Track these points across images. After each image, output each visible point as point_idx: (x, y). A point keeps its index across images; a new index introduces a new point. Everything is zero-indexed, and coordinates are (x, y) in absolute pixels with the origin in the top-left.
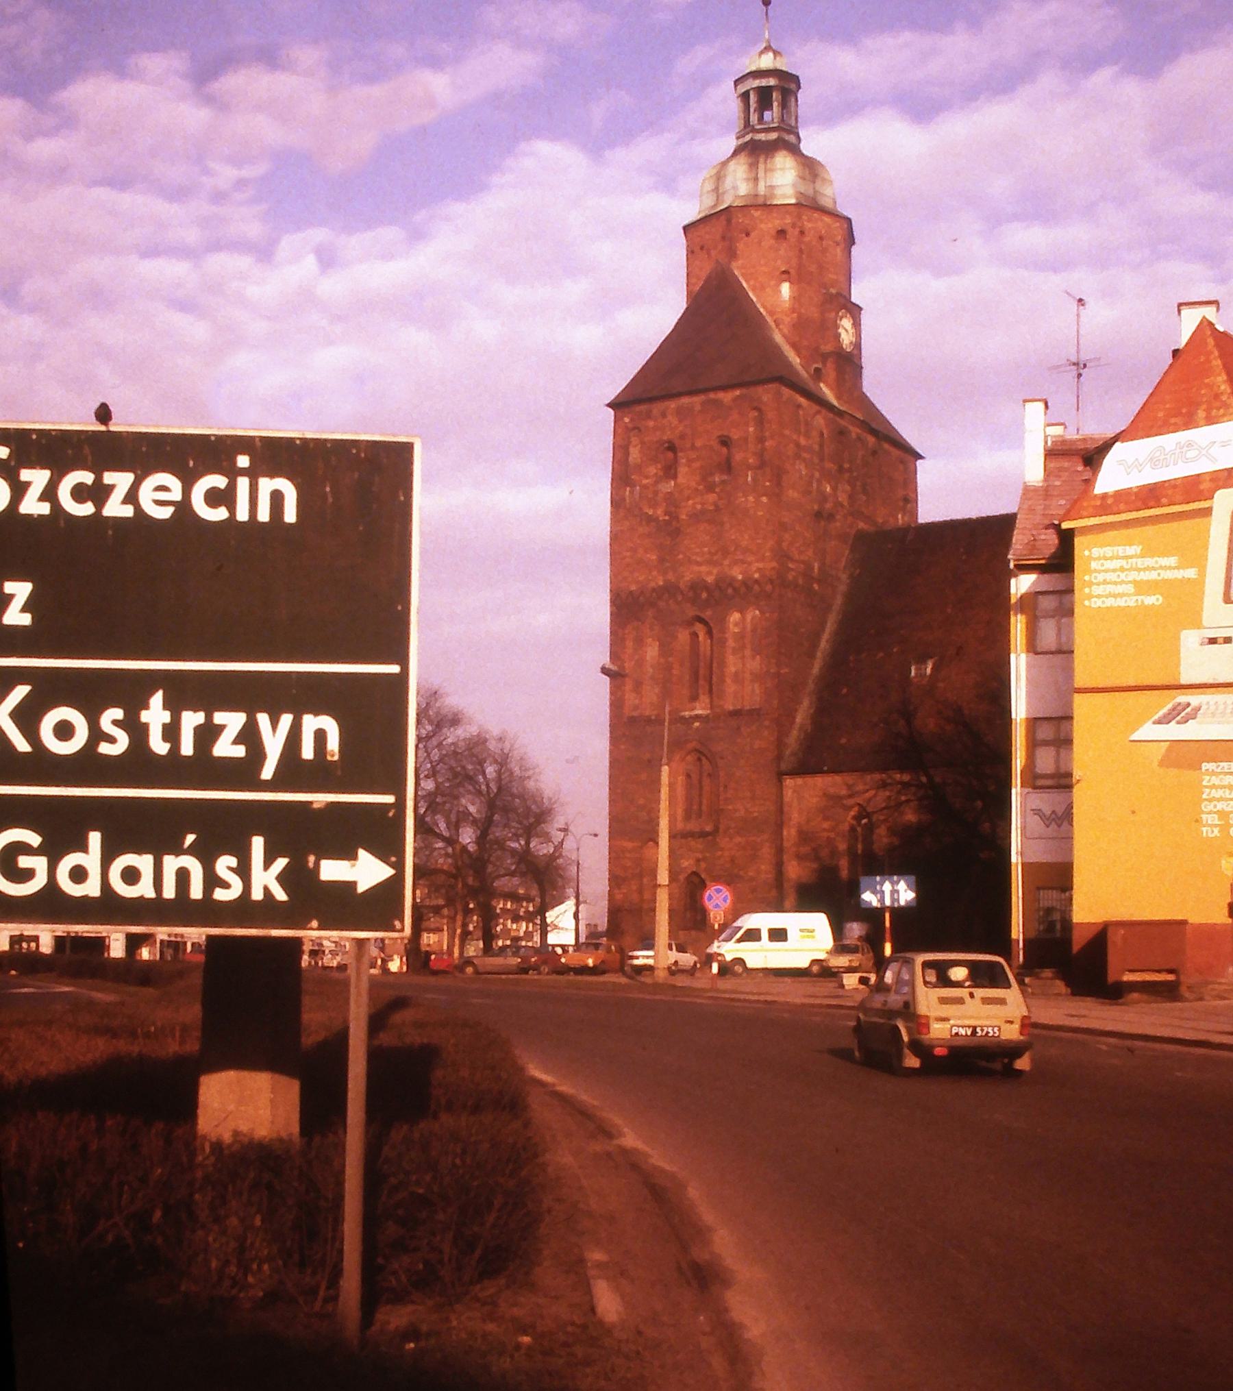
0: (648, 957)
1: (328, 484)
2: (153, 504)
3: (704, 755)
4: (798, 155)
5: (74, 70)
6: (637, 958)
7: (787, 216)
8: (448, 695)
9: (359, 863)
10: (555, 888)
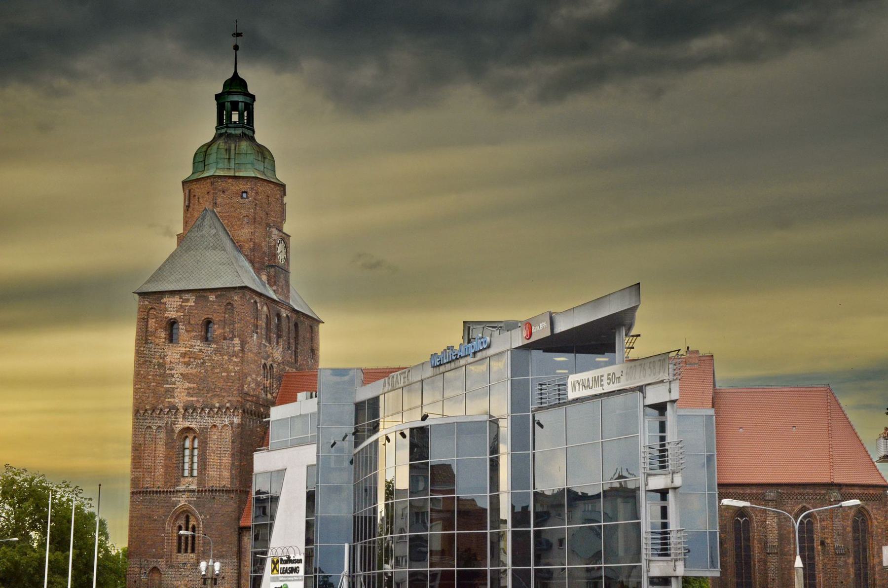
0: (192, 470)
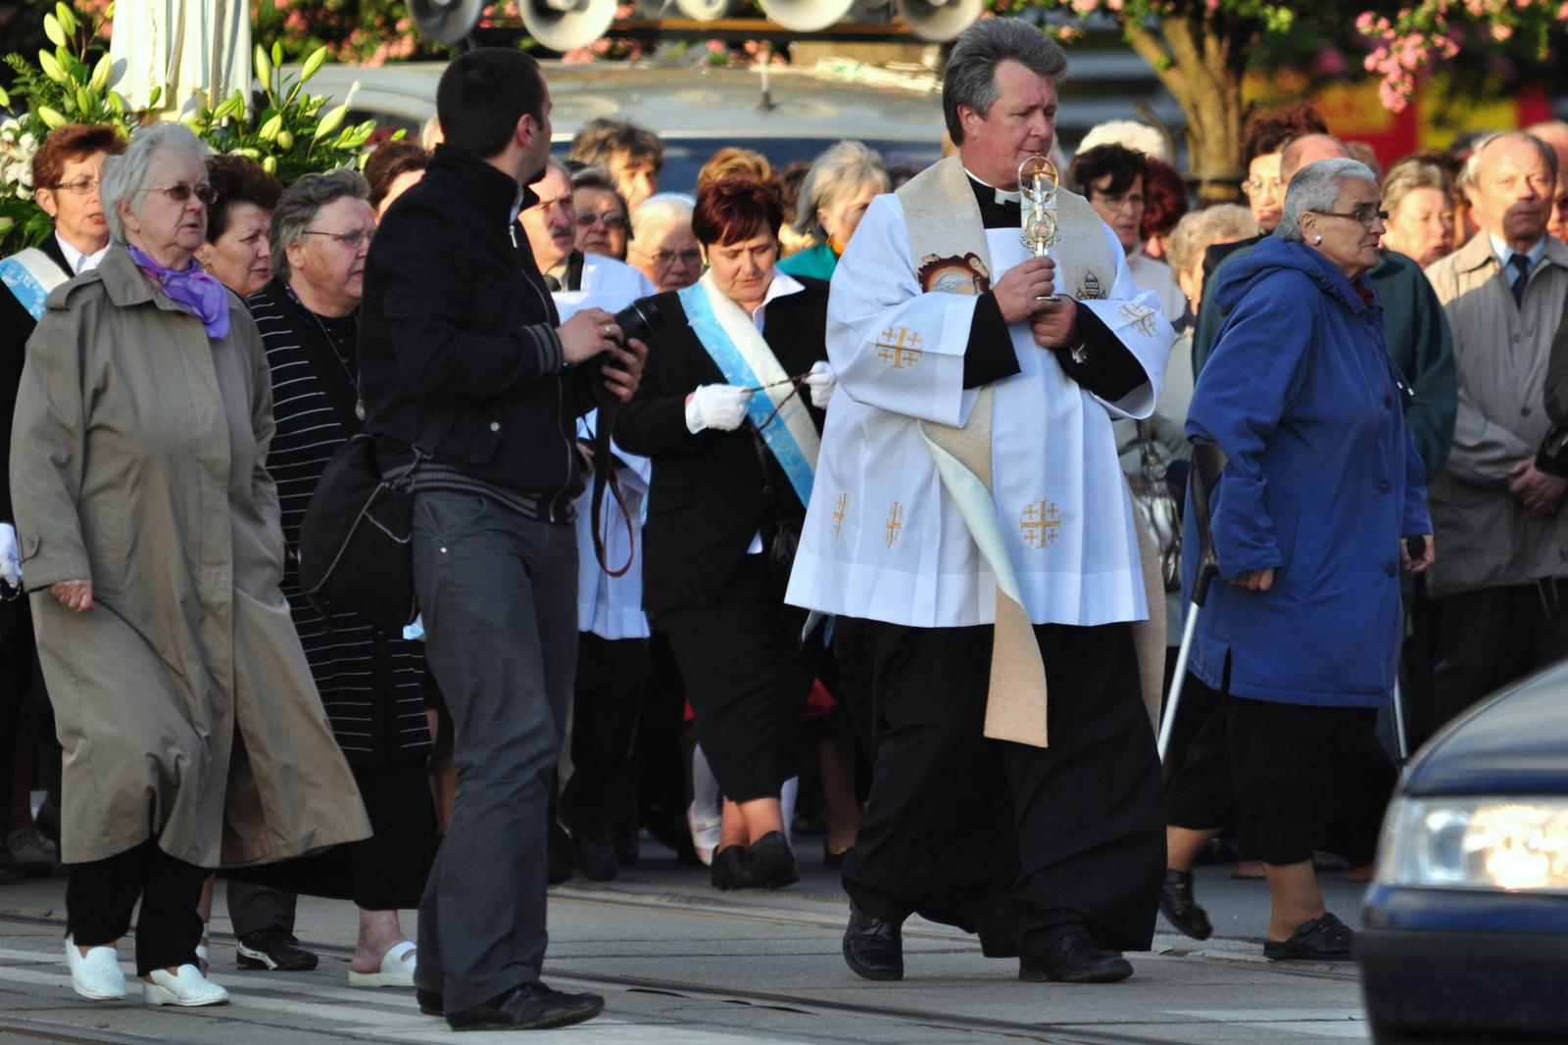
1: (570, 836)
3: (279, 81)
4: (1433, 254)
5: (381, 955)
7: (396, 474)
9: (1387, 209)
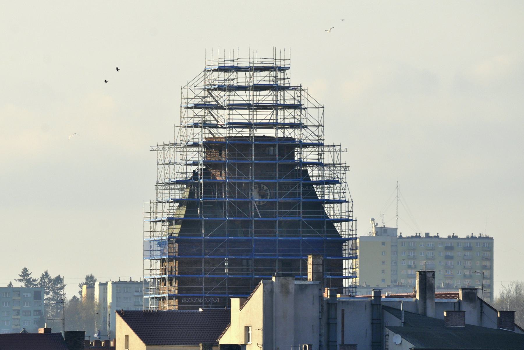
2: (105, 81)
6: (227, 149)
8: (88, 275)
10: (500, 300)
